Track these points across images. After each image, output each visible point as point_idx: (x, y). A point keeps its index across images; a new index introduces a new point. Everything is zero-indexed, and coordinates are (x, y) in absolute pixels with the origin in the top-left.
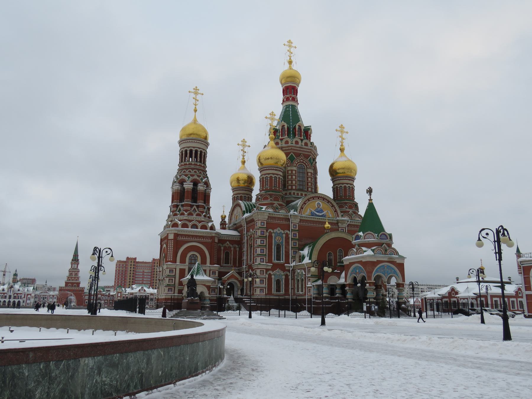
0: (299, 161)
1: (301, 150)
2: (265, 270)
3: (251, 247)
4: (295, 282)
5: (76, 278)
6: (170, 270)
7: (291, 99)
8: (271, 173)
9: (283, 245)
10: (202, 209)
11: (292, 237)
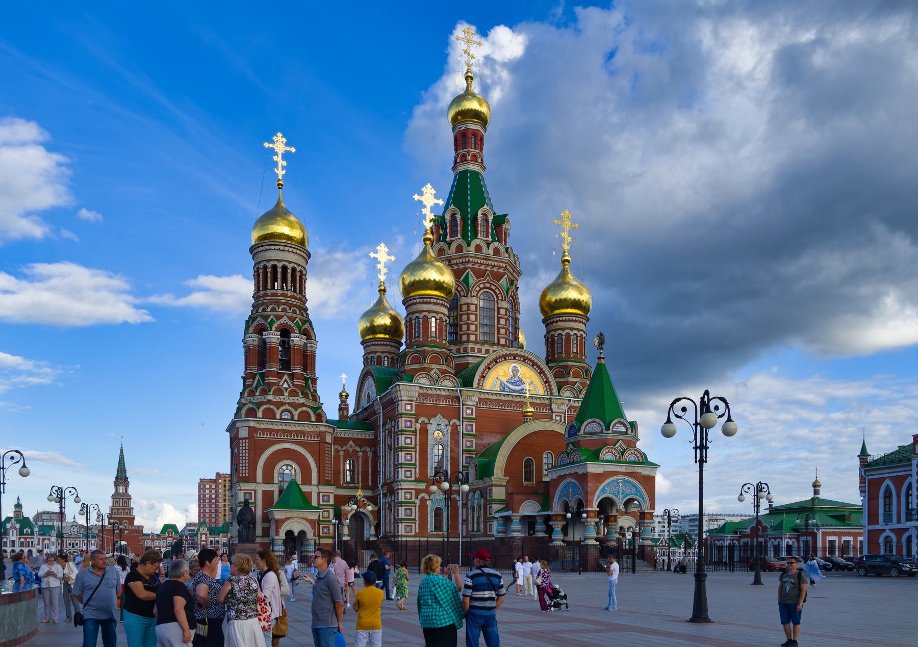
0: (482, 286)
1: (486, 264)
2: (413, 491)
3: (391, 449)
5: (127, 511)
7: (469, 158)
10: (300, 381)
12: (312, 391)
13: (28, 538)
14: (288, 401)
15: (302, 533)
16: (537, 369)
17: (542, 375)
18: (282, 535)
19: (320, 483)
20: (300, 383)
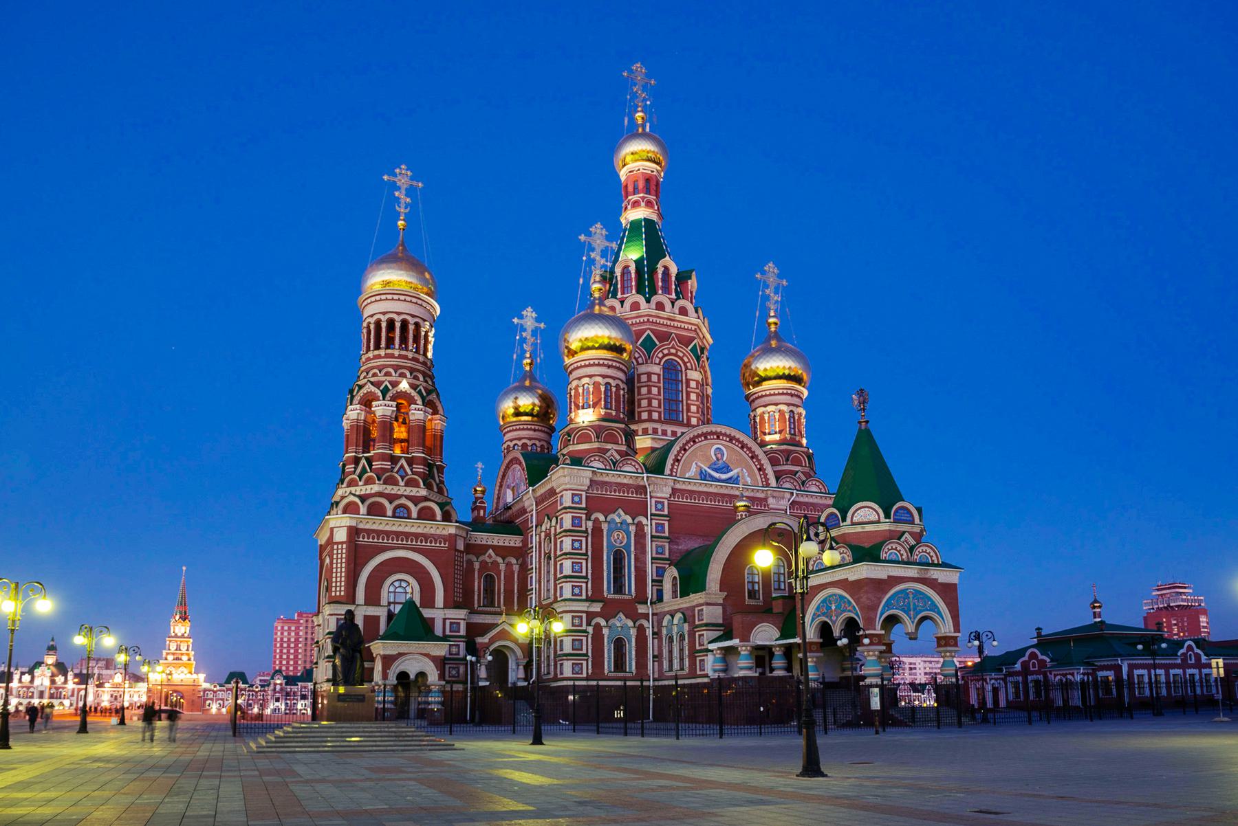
2: (584, 615)
3: (549, 558)
4: (662, 644)
8: (596, 373)
9: (631, 552)
11: (654, 534)
12: (438, 481)
14: (405, 493)
15: (422, 675)
16: (748, 452)
19: (446, 606)
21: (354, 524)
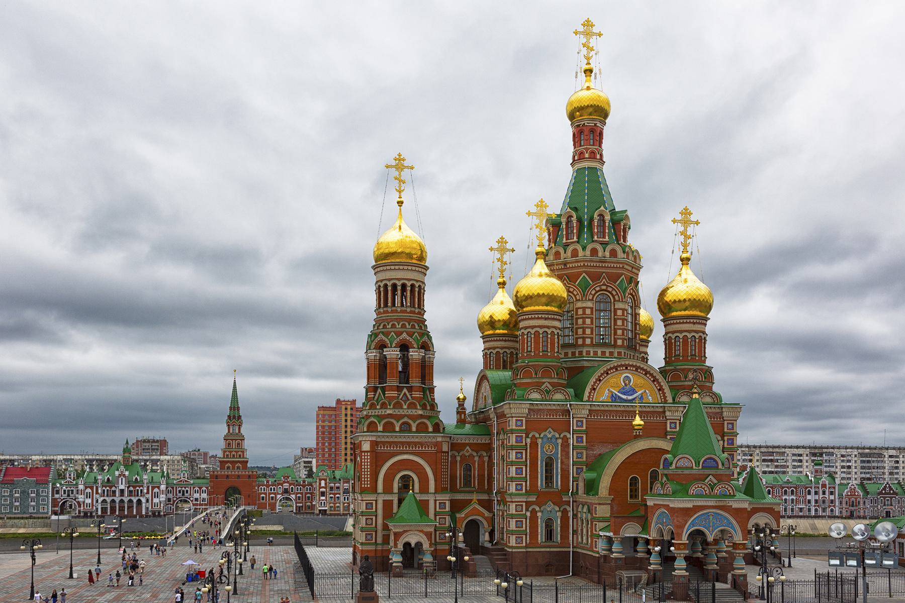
0: (598, 289)
2: (524, 504)
6: (367, 504)
7: (587, 155)
10: (418, 393)
13: (137, 486)
15: (419, 544)
16: (650, 377)
17: (655, 383)
18: (400, 547)
20: (418, 396)
21: (374, 439)
